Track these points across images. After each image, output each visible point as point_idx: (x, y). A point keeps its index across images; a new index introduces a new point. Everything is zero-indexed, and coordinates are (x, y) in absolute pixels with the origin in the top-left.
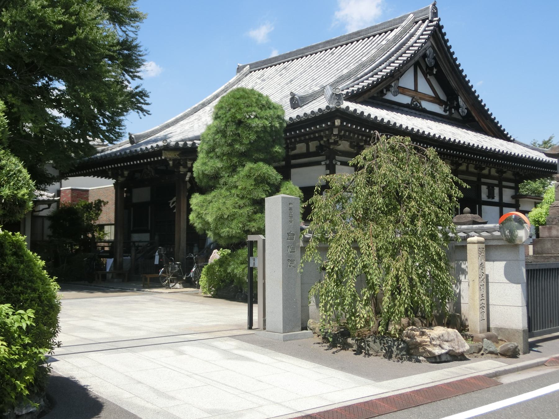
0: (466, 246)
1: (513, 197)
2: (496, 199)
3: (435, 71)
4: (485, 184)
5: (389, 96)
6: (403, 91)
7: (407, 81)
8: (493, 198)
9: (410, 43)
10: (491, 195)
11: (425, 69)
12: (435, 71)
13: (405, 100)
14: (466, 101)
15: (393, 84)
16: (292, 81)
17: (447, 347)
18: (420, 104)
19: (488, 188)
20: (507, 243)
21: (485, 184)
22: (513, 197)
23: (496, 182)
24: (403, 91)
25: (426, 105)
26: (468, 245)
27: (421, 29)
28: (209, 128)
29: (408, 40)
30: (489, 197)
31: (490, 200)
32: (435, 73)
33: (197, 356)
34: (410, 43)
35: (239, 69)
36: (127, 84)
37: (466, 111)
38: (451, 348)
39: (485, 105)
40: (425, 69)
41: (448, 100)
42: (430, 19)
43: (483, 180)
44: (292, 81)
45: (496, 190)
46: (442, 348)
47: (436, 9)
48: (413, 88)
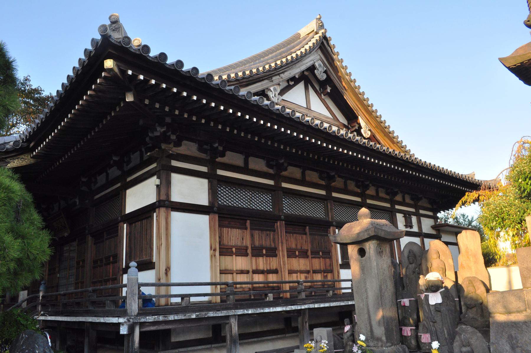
1: (433, 227)
2: (415, 229)
3: (329, 90)
4: (400, 211)
8: (411, 227)
10: (409, 224)
11: (318, 90)
12: (329, 90)
14: (368, 122)
16: (243, 239)
19: (405, 217)
20: (440, 228)
21: (400, 211)
22: (433, 227)
23: (413, 210)
28: (9, 58)
30: (406, 226)
31: (408, 229)
32: (329, 91)
37: (369, 133)
40: (318, 90)
41: (348, 124)
43: (397, 207)
44: (243, 239)
45: (414, 219)
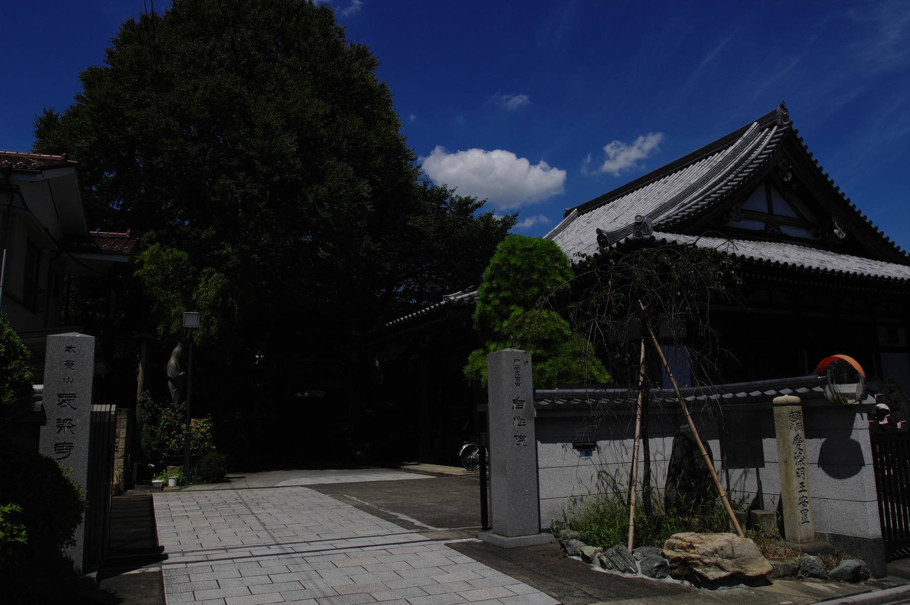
0: (772, 410)
5: (733, 224)
6: (754, 216)
7: (758, 203)
9: (753, 156)
13: (759, 226)
15: (734, 208)
17: (731, 568)
18: (779, 229)
24: (754, 216)
25: (784, 230)
26: (776, 409)
27: (771, 135)
29: (751, 152)
33: (417, 547)
34: (753, 156)
35: (567, 213)
36: (40, 403)
38: (737, 569)
39: (871, 222)
42: (779, 123)
46: (722, 569)
47: (786, 110)
48: (766, 211)
